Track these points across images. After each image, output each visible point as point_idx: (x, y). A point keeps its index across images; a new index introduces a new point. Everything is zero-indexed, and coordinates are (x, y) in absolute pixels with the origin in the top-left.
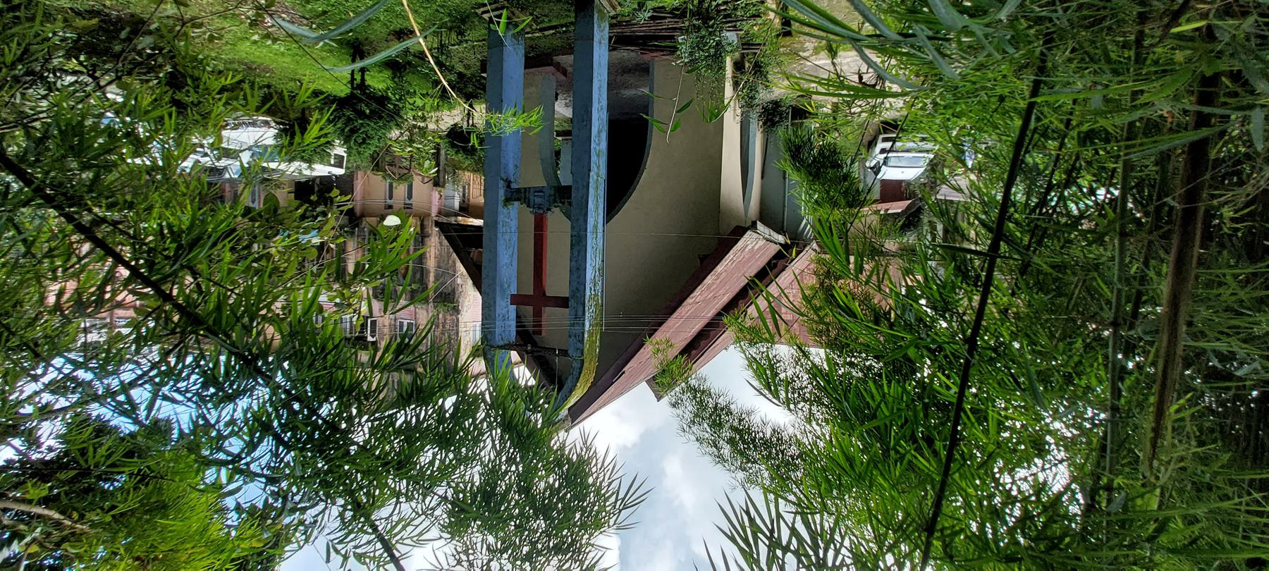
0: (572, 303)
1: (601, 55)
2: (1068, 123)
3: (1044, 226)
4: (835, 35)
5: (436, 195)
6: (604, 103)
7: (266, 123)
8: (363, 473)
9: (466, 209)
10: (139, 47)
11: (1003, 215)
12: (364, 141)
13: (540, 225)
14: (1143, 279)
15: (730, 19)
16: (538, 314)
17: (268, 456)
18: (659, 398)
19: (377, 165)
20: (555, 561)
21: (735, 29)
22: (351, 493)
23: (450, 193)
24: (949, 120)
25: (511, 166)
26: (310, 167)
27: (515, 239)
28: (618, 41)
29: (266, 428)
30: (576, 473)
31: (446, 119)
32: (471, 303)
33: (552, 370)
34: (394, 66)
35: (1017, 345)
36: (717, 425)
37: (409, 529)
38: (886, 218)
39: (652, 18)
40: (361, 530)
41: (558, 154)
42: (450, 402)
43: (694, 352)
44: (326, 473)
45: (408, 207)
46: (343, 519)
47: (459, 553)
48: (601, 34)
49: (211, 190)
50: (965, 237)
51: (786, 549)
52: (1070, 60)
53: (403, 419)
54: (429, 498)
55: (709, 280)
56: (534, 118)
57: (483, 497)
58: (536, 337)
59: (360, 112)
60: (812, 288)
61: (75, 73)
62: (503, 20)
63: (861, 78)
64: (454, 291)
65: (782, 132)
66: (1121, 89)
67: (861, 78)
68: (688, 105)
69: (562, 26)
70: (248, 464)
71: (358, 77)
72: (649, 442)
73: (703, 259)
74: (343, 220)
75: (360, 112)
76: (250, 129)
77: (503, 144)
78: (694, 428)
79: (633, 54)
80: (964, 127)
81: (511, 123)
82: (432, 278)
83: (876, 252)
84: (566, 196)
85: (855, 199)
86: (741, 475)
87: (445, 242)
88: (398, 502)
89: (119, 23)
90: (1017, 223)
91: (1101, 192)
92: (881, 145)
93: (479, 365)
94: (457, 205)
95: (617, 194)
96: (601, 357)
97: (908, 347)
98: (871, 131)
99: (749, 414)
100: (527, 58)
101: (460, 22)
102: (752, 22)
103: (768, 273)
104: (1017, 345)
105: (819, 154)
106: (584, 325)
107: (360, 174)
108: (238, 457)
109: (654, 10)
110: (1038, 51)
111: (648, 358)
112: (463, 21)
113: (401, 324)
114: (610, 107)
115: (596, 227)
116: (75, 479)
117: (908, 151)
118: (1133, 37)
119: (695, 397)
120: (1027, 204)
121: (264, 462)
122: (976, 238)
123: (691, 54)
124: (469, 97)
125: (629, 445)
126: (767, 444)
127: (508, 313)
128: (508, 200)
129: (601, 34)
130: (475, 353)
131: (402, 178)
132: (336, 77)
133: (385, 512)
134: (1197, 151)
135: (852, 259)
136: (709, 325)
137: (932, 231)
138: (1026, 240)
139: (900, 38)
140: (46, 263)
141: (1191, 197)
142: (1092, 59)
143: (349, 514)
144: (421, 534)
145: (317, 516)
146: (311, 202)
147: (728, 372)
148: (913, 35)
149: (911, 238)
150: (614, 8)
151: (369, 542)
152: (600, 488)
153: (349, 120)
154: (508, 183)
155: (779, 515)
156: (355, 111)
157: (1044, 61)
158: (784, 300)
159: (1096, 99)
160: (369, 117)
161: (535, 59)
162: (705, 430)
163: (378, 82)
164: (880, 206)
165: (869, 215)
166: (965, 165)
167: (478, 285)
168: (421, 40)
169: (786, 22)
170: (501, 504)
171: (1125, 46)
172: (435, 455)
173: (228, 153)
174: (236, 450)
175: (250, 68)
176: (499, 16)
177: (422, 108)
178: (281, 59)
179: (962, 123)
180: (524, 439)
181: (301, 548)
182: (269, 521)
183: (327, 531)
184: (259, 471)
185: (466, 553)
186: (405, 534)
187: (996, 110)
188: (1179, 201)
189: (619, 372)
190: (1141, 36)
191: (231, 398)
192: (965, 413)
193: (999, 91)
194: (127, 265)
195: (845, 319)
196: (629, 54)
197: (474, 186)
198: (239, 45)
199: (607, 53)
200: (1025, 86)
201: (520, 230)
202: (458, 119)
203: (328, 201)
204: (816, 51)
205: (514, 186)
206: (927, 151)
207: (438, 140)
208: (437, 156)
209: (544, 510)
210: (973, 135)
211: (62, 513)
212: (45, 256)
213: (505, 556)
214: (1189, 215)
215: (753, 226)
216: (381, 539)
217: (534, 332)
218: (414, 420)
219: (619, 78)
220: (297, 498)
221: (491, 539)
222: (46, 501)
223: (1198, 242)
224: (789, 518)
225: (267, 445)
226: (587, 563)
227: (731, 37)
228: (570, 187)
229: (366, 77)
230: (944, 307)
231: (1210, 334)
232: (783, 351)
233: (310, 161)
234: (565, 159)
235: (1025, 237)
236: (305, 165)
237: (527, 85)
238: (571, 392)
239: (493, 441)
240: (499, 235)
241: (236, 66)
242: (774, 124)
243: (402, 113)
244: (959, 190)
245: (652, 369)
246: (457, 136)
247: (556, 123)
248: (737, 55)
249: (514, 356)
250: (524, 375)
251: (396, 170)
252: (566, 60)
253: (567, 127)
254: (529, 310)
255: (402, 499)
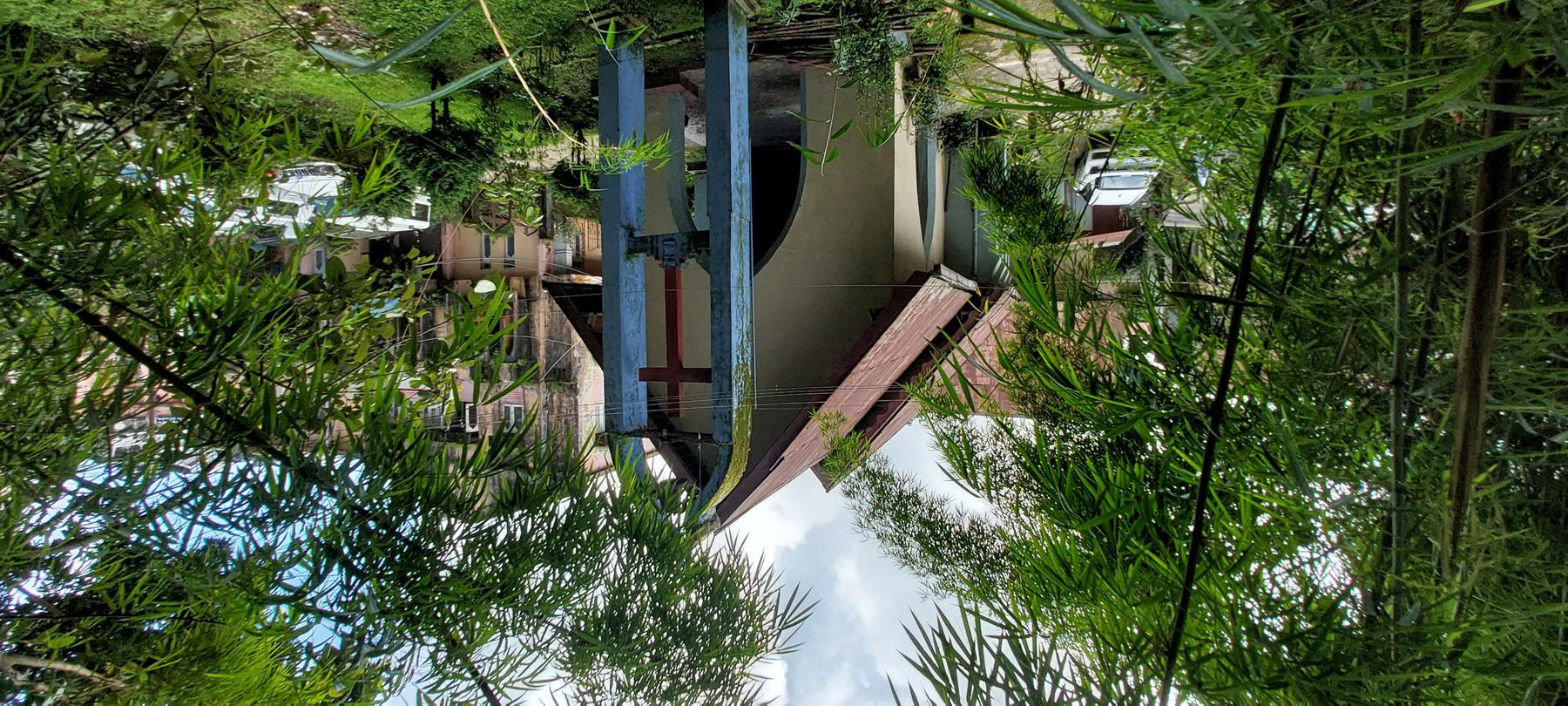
0: (714, 375)
1: (739, 68)
2: (1327, 130)
3: (1305, 257)
4: (1026, 34)
5: (543, 249)
6: (746, 126)
7: (331, 169)
8: (458, 603)
9: (580, 264)
10: (160, 84)
11: (1250, 250)
12: (451, 187)
13: (672, 281)
14: (1429, 325)
15: (896, 15)
16: (674, 391)
17: (338, 588)
18: (828, 486)
19: (469, 215)
20: (702, 699)
21: (905, 27)
22: (442, 630)
23: (561, 245)
24: (1174, 129)
25: (633, 210)
26: (386, 221)
27: (642, 299)
28: (760, 48)
29: (333, 553)
30: (723, 587)
31: (551, 154)
32: (591, 380)
33: (694, 458)
34: (487, 93)
35: (1272, 407)
36: (902, 518)
37: (520, 669)
38: (1100, 252)
39: (800, 18)
40: (456, 676)
41: (691, 191)
42: (564, 505)
43: (869, 429)
44: (411, 606)
45: (509, 264)
46: (435, 662)
47: (582, 694)
48: (738, 41)
49: (269, 255)
50: (1200, 275)
51: (991, 681)
52: (1329, 53)
53: (505, 532)
54: (542, 629)
55: (884, 340)
56: (658, 150)
57: (609, 625)
58: (672, 420)
59: (443, 151)
60: (1013, 344)
61: (91, 118)
62: (611, 32)
63: (1062, 84)
64: (570, 366)
65: (964, 152)
66: (1398, 87)
67: (1062, 84)
68: (846, 128)
69: (689, 33)
70: (313, 600)
71: (440, 107)
72: (816, 544)
73: (875, 314)
74: (429, 284)
75: (443, 151)
76: (311, 177)
77: (622, 183)
78: (875, 523)
79: (779, 65)
80: (1194, 137)
81: (630, 157)
82: (542, 352)
83: (1089, 296)
84: (703, 244)
85: (1057, 230)
86: (933, 579)
87: (557, 307)
88: (503, 636)
89: (133, 56)
90: (1266, 255)
91: (1371, 212)
92: (1091, 163)
93: (599, 457)
94: (569, 259)
95: (767, 235)
96: (753, 442)
97: (1133, 421)
98: (1077, 151)
99: (942, 503)
100: (648, 75)
101: (563, 34)
102: (925, 17)
103: (959, 325)
104: (1272, 407)
105: (1012, 178)
106: (731, 402)
107: (449, 226)
108: (299, 593)
109: (803, 7)
110: (1286, 42)
111: (814, 437)
112: (566, 32)
113: (507, 409)
114: (753, 132)
115: (741, 280)
116: (96, 623)
117: (1125, 169)
118: (1406, 16)
119: (874, 484)
120: (1279, 232)
121: (332, 597)
122: (1216, 283)
123: (851, 60)
124: (579, 128)
125: (793, 547)
126: (965, 539)
127: (636, 392)
128: (631, 252)
129: (738, 41)
130: (602, 440)
131: (499, 230)
132: (413, 110)
133: (488, 649)
134: (1497, 162)
135: (1060, 306)
136: (884, 396)
137: (1153, 274)
138: (1279, 275)
139: (1108, 34)
140: (48, 362)
141: (1491, 221)
142: (1356, 48)
143: (442, 655)
144: (534, 674)
145: (405, 658)
146: (384, 267)
147: (913, 451)
148: (1126, 30)
149: (1132, 277)
150: (752, 7)
151: (469, 688)
152: (753, 605)
153: (432, 162)
154: (631, 231)
155: (982, 642)
156: (438, 150)
157: (1295, 54)
158: (979, 360)
159: (1363, 100)
160: (455, 158)
161: (658, 76)
162: (888, 524)
163: (466, 113)
164: (1091, 239)
165: (1080, 251)
166: (1197, 183)
167: (598, 358)
168: (511, 61)
169: (968, 19)
170: (632, 631)
171: (1395, 27)
172: (546, 575)
173: (278, 208)
174: (296, 583)
175: (307, 103)
176: (606, 27)
177: (521, 143)
178: (344, 90)
179: (1191, 132)
180: (662, 548)
181: (386, 699)
182: (348, 665)
183: (416, 677)
184: (327, 608)
185: (591, 692)
186: (515, 675)
187: (1234, 115)
188: (1468, 235)
189: (776, 459)
190: (1415, 22)
191: (291, 518)
192: (1211, 497)
193: (1239, 94)
194: (148, 361)
195: (1052, 385)
196: (773, 64)
197: (589, 236)
198: (296, 76)
199: (745, 64)
200: (1269, 84)
201: (647, 286)
202: (567, 155)
203: (406, 265)
204: (1006, 51)
205: (637, 234)
206: (1150, 168)
207: (542, 182)
208: (542, 201)
209: (686, 635)
210: (1206, 147)
211: (90, 667)
212: (49, 352)
213: (640, 694)
214: (1489, 245)
215: (936, 271)
216: (483, 684)
217: (671, 414)
218: (519, 533)
219: (763, 94)
220: (376, 640)
221: (621, 674)
222: (64, 654)
223: (1501, 277)
224: (993, 643)
225: (335, 575)
226: (742, 697)
227: (900, 37)
228: (707, 233)
229: (451, 108)
230: (1179, 362)
231: (1520, 392)
232: (981, 423)
233: (386, 215)
234: (700, 197)
235: (1277, 271)
236: (380, 219)
237: (649, 108)
238: (718, 485)
239: (619, 554)
240: (622, 296)
241: (289, 101)
242: (957, 143)
243: (496, 150)
244: (1191, 216)
245: (820, 452)
246: (564, 176)
247: (687, 153)
248: (908, 59)
249: (647, 444)
250: (660, 468)
251: (492, 221)
252: (696, 75)
253: (700, 158)
254: (662, 386)
255: (509, 632)
